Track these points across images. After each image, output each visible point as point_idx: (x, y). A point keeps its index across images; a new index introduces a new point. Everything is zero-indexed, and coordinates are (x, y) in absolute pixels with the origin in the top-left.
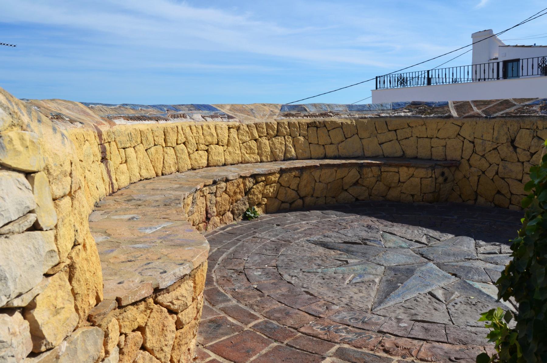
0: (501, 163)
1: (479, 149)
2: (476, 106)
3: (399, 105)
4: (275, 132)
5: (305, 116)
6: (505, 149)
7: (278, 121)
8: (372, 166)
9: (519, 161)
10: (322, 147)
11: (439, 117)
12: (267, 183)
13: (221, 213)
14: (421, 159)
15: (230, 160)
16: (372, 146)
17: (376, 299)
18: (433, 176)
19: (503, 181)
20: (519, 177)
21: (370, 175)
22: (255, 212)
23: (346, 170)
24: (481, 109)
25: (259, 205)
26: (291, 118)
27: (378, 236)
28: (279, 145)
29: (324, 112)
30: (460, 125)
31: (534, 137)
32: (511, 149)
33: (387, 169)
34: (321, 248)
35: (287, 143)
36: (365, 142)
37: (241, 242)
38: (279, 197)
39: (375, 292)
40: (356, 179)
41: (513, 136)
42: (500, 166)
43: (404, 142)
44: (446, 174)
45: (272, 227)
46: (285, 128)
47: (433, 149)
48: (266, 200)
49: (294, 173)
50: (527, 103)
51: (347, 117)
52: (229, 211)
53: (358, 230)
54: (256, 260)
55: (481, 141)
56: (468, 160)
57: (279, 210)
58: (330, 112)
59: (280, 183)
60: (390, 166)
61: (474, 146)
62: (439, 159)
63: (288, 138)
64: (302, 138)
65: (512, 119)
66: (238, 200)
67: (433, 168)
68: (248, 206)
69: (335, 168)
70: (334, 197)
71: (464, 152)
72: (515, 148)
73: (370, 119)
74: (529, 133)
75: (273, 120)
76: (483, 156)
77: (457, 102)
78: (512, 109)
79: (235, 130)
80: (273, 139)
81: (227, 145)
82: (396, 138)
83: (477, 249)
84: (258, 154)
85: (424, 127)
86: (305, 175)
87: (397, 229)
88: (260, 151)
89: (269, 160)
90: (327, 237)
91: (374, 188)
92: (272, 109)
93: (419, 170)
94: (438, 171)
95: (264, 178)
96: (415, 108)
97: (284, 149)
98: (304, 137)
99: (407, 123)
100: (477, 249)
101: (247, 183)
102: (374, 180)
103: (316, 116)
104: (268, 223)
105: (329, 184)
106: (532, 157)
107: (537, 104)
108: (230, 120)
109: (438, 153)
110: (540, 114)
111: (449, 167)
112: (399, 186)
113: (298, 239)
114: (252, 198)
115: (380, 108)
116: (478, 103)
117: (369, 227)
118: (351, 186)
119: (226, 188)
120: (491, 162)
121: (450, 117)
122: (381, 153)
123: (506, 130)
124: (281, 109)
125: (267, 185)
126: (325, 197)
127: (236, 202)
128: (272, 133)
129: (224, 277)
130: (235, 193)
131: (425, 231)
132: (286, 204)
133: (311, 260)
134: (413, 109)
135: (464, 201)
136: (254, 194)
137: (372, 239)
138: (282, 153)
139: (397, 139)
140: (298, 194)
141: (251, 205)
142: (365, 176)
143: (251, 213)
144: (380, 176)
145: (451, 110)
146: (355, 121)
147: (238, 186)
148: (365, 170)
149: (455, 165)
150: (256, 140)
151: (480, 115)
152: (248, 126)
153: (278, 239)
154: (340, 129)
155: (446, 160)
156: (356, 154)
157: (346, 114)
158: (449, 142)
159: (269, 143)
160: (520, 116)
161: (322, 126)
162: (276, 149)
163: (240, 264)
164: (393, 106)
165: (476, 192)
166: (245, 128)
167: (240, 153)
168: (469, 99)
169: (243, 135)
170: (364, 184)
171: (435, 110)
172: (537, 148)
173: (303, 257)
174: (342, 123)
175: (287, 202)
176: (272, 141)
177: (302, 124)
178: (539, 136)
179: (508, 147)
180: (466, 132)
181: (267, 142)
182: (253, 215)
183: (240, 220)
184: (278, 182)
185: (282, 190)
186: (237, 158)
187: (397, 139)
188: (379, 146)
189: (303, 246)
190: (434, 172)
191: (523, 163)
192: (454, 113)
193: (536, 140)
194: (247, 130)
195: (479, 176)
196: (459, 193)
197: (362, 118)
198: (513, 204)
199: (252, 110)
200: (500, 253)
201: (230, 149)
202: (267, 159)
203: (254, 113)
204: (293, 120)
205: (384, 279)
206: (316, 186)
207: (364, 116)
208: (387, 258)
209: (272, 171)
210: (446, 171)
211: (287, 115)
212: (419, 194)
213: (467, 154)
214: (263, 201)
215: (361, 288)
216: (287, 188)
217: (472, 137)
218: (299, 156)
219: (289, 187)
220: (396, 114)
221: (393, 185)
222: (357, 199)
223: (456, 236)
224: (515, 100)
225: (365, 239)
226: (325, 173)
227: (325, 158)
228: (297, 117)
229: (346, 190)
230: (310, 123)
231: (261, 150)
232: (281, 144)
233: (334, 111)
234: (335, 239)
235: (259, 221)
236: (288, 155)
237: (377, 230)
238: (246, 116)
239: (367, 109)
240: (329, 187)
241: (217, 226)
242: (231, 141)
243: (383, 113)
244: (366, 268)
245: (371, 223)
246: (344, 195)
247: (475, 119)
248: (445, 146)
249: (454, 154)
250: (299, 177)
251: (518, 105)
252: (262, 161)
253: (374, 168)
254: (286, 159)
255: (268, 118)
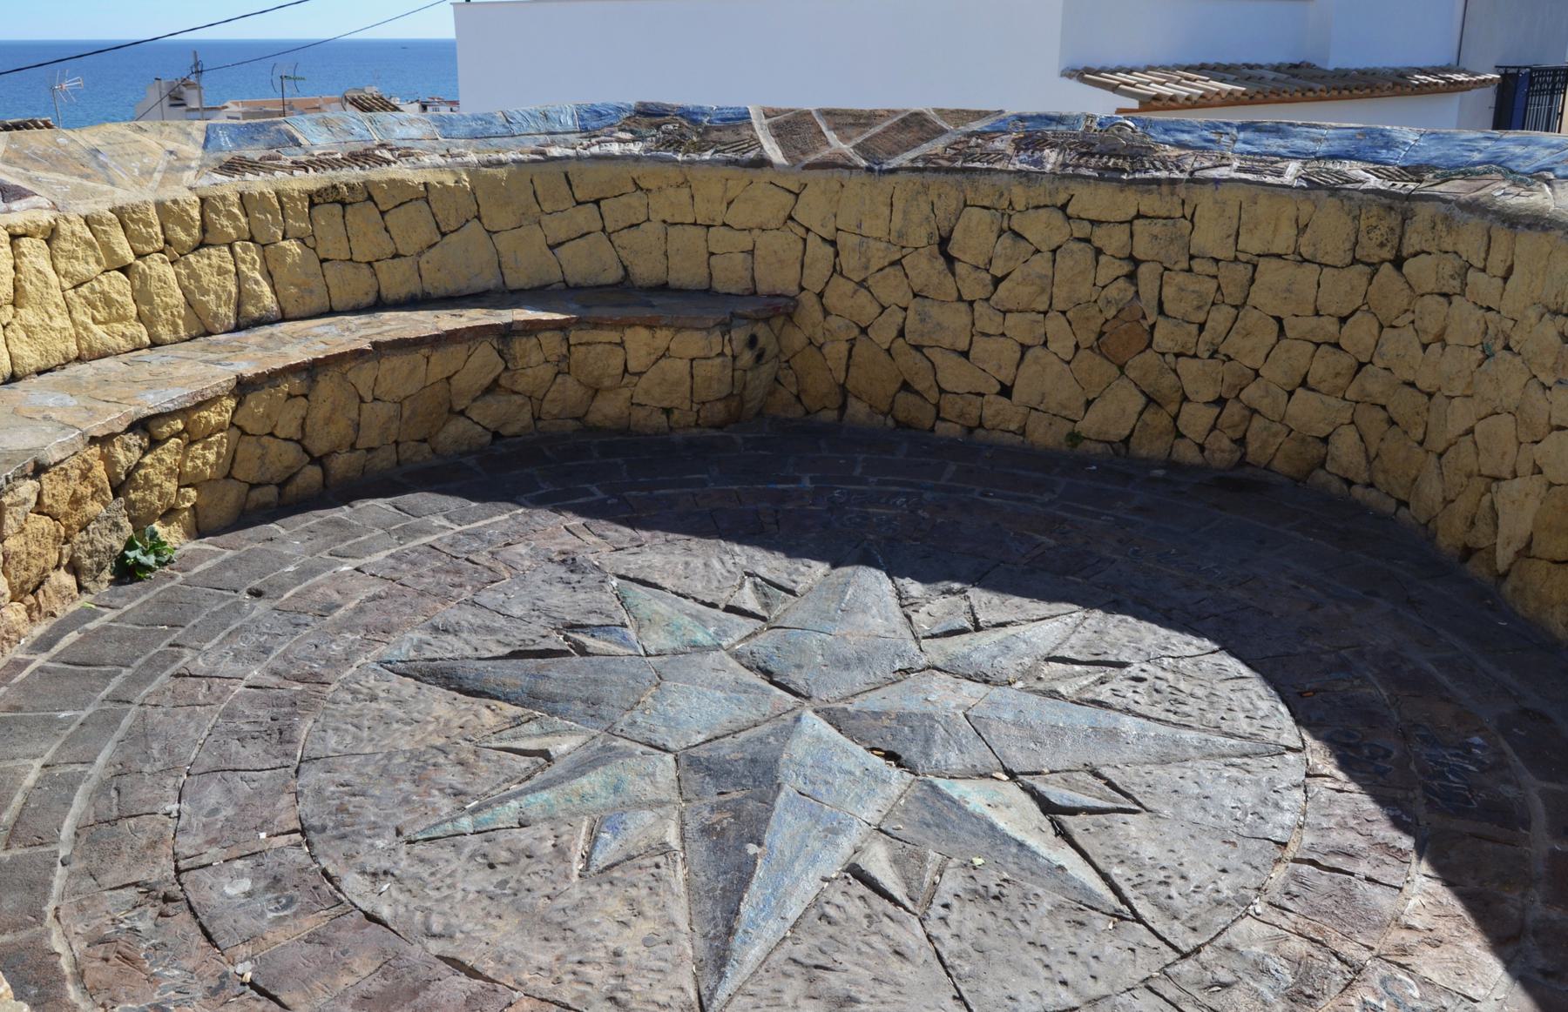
0: (914, 305)
1: (849, 262)
2: (835, 129)
3: (600, 115)
4: (196, 232)
5: (297, 165)
6: (924, 264)
7: (203, 194)
8: (541, 330)
9: (960, 299)
10: (366, 270)
11: (729, 162)
12: (192, 437)
13: (30, 586)
14: (681, 292)
15: (31, 357)
16: (527, 259)
17: (699, 942)
18: (728, 351)
19: (918, 355)
20: (963, 345)
21: (536, 357)
22: (157, 547)
23: (459, 351)
24: (850, 139)
25: (169, 515)
26: (249, 176)
27: (607, 600)
28: (215, 279)
29: (359, 148)
30: (795, 189)
31: (1001, 232)
32: (940, 263)
33: (586, 336)
34: (439, 691)
35: (243, 267)
36: (502, 241)
37: (134, 709)
38: (239, 473)
39: (684, 901)
40: (492, 376)
41: (945, 226)
42: (910, 313)
43: (624, 238)
44: (762, 341)
45: (237, 608)
46: (231, 216)
47: (713, 259)
48: (192, 493)
49: (285, 387)
50: (977, 126)
51: (441, 161)
52: (58, 567)
53: (538, 578)
54: (215, 811)
55: (856, 239)
56: (821, 295)
57: (245, 518)
58: (383, 146)
59: (239, 427)
60: (597, 325)
61: (837, 254)
62: (733, 291)
63: (245, 250)
64: (293, 246)
65: (942, 177)
66: (89, 522)
67: (726, 327)
68: (128, 527)
69: (425, 351)
70: (425, 441)
71: (806, 271)
72: (950, 261)
73: (514, 167)
74: (988, 220)
75: (182, 192)
76: (862, 284)
77: (777, 112)
78: (937, 146)
79: (39, 242)
80: (191, 258)
81: (14, 304)
82: (600, 226)
83: (908, 617)
84: (139, 318)
85: (685, 192)
86: (326, 386)
87: (658, 560)
88: (145, 308)
89: (183, 334)
90: (446, 631)
91: (549, 396)
92: (171, 146)
93: (686, 335)
94: (739, 335)
95: (179, 425)
96: (651, 125)
97: (234, 290)
98: (302, 240)
99: (634, 179)
100: (908, 617)
101: (119, 453)
102: (547, 372)
103: (334, 164)
104: (212, 581)
105: (407, 403)
106: (996, 289)
107: (1005, 133)
108: (15, 205)
109: (730, 274)
110: (1018, 166)
111: (767, 320)
112: (626, 386)
113: (348, 659)
114: (143, 500)
115: (543, 126)
116: (838, 120)
117: (569, 562)
118: (474, 400)
119: (40, 495)
120: (885, 301)
121: (762, 163)
122: (556, 275)
123: (926, 208)
124: (207, 140)
125: (192, 442)
126: (397, 443)
127: (83, 528)
128: (182, 236)
129: (103, 941)
130: (76, 501)
131: (744, 555)
132: (265, 490)
133: (420, 770)
134: (644, 131)
135: (808, 413)
136: (148, 484)
137: (594, 620)
138: (227, 304)
139: (604, 230)
140: (305, 450)
141: (140, 523)
142: (521, 364)
143: (145, 554)
144: (566, 358)
145: (762, 140)
146: (469, 174)
147: (84, 476)
148: (519, 345)
149: (782, 308)
150: (125, 270)
151: (850, 160)
152: (88, 221)
153: (275, 673)
154: (423, 205)
155: (755, 293)
156: (479, 284)
157: (434, 150)
158: (763, 240)
159: (178, 274)
160: (964, 170)
161: (360, 198)
162: (205, 292)
163: (153, 845)
164: (581, 119)
165: (843, 387)
166: (77, 228)
167: (68, 323)
168: (811, 104)
169: (72, 256)
170: (518, 388)
171: (714, 135)
172: (1012, 264)
173: (389, 756)
174: (425, 184)
175: (268, 484)
176: (188, 265)
177: (290, 197)
178: (1016, 228)
179: (932, 257)
180: (812, 211)
181: (169, 272)
182: (150, 560)
183: (104, 587)
184: (232, 424)
185: (249, 449)
186: (62, 347)
187: (604, 230)
188: (549, 253)
189: (374, 698)
190: (730, 340)
191: (971, 303)
192: (775, 153)
193: (1007, 239)
194: (90, 235)
195: (852, 342)
196: (794, 390)
197: (489, 164)
198: (944, 420)
199: (95, 152)
200: (978, 628)
201: (29, 315)
202: (176, 332)
203: (104, 166)
204: (257, 183)
205: (693, 825)
206: (365, 414)
207: (495, 156)
208: (671, 712)
209: (209, 394)
210: (762, 331)
211: (231, 167)
212: (686, 405)
213: (814, 280)
214: (185, 498)
215: (633, 892)
216: (265, 439)
217: (831, 228)
218: (291, 310)
219: (271, 434)
220: (595, 150)
221: (607, 382)
222: (496, 435)
223: (834, 566)
224: (940, 112)
225: (572, 627)
226: (393, 369)
227: (380, 304)
228: (271, 171)
229: (462, 413)
230: (319, 193)
231: (150, 302)
232: (222, 272)
233: (396, 144)
234: (474, 639)
235: (180, 576)
236: (251, 309)
237: (596, 575)
238: (76, 180)
239: (501, 130)
240: (406, 413)
241: (20, 636)
242: (28, 287)
243: (553, 144)
244: (620, 780)
245: (569, 543)
246: (457, 427)
247: (837, 173)
248: (752, 252)
249: (777, 278)
250: (305, 396)
251: (955, 132)
252: (155, 343)
253: (548, 338)
254: (244, 324)
255: (162, 184)
